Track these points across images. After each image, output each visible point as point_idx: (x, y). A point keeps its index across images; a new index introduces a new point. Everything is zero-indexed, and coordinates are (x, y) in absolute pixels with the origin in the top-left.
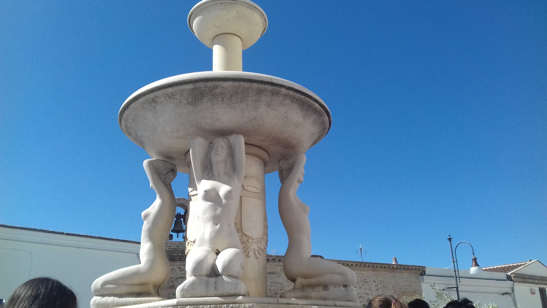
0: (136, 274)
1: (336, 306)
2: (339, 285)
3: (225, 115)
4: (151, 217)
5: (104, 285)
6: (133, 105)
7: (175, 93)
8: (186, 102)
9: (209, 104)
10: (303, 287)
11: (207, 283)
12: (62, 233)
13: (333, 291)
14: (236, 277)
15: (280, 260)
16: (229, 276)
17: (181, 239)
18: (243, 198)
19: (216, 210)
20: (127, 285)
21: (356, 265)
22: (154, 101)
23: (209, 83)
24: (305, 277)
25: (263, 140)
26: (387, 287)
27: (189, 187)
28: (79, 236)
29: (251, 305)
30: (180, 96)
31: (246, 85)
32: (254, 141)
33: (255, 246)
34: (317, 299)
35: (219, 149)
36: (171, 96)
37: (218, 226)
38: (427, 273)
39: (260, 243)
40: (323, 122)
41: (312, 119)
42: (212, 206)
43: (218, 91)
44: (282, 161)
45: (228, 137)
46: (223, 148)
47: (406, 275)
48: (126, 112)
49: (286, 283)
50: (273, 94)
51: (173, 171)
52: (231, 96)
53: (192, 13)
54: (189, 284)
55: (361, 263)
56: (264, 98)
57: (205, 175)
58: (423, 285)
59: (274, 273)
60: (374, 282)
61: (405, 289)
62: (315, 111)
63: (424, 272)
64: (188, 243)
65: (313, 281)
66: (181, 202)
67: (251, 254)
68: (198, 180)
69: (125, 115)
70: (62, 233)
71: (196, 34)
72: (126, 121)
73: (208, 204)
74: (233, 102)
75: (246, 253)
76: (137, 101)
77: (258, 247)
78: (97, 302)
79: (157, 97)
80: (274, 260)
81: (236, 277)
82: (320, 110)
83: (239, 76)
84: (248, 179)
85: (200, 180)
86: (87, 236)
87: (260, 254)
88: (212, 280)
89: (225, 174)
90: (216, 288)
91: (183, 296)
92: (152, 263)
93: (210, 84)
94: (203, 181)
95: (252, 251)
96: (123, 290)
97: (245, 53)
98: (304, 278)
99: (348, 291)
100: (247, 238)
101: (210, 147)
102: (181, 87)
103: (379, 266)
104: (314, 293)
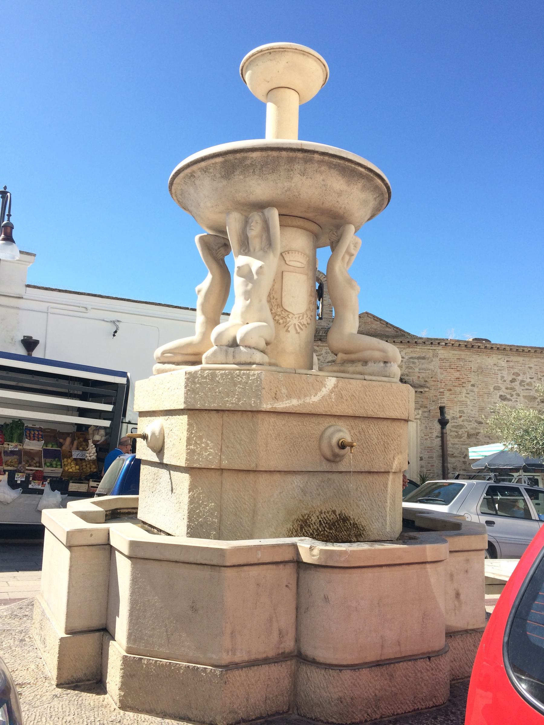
0: (189, 345)
1: (365, 380)
3: (259, 188)
4: (203, 293)
6: (177, 180)
7: (209, 167)
8: (220, 176)
9: (241, 177)
10: (344, 362)
11: (227, 352)
12: (187, 309)
13: (371, 367)
14: (250, 347)
15: (432, 343)
18: (283, 254)
19: (247, 285)
21: (535, 351)
22: (192, 175)
23: (238, 154)
24: (346, 352)
25: (305, 211)
29: (259, 372)
31: (275, 154)
33: (296, 322)
34: (353, 373)
36: (205, 170)
37: (249, 300)
39: (303, 318)
41: (360, 185)
42: (244, 281)
43: (248, 162)
49: (439, 370)
50: (306, 161)
52: (262, 166)
53: (243, 67)
56: (296, 166)
57: (242, 251)
59: (424, 358)
65: (353, 356)
70: (187, 309)
71: (250, 89)
73: (242, 279)
74: (265, 173)
75: (286, 328)
77: (300, 322)
79: (194, 172)
80: (424, 343)
81: (250, 347)
82: (367, 174)
83: (267, 145)
84: (290, 254)
85: (237, 256)
88: (231, 350)
89: (261, 249)
90: (234, 357)
91: (207, 363)
93: (238, 156)
95: (292, 325)
96: (179, 358)
97: (301, 107)
99: (386, 367)
100: (287, 313)
101: (246, 222)
104: (351, 368)
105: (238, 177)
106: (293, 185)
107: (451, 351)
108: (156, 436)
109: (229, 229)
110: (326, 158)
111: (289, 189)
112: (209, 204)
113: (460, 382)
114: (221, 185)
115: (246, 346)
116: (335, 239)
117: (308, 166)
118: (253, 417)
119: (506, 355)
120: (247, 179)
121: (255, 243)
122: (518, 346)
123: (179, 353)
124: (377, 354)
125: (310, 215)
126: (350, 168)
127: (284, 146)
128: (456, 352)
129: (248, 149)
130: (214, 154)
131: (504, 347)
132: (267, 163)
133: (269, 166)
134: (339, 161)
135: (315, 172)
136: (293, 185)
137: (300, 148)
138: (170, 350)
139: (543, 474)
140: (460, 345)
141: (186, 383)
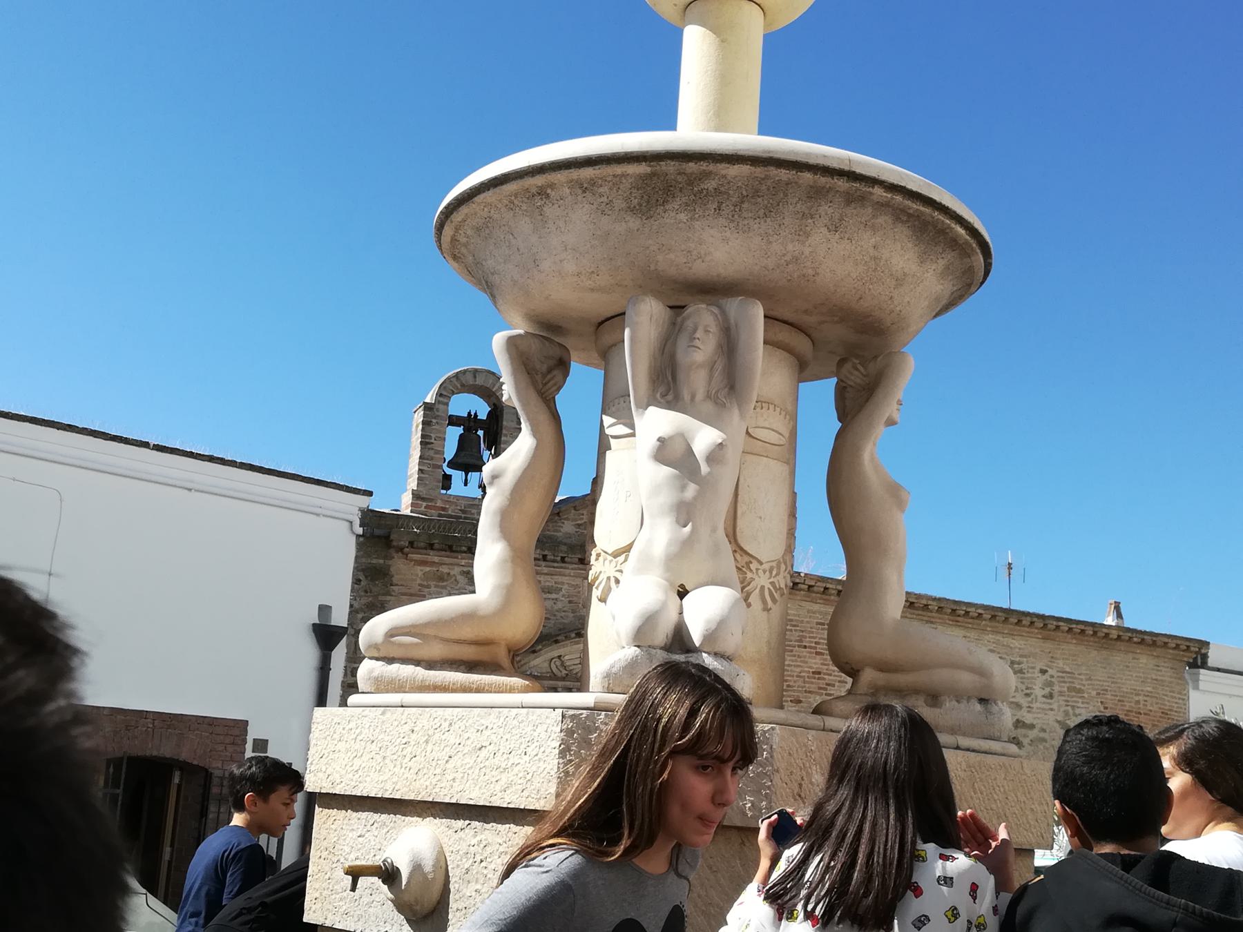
0: (469, 617)
1: (958, 748)
2: (969, 699)
3: (721, 248)
4: (508, 480)
5: (392, 636)
9: (683, 216)
12: (145, 445)
16: (716, 655)
17: (473, 491)
19: (683, 488)
20: (447, 641)
21: (994, 617)
22: (542, 192)
24: (884, 667)
25: (806, 312)
26: (1080, 691)
27: (604, 412)
28: (191, 455)
30: (611, 189)
31: (784, 174)
32: (787, 314)
35: (697, 335)
36: (586, 188)
37: (688, 528)
38: (1211, 662)
40: (970, 270)
41: (942, 263)
42: (676, 477)
44: (848, 366)
45: (723, 302)
46: (707, 331)
47: (1144, 661)
48: (464, 210)
50: (851, 199)
51: (563, 365)
54: (623, 664)
55: (1009, 612)
57: (658, 395)
58: (1193, 694)
60: (1043, 672)
61: (1138, 702)
62: (954, 243)
63: (1205, 657)
64: (598, 555)
66: (480, 381)
67: (754, 599)
68: (638, 407)
69: (457, 217)
70: (145, 445)
72: (457, 229)
73: (666, 471)
76: (497, 190)
78: (375, 674)
79: (552, 186)
82: (967, 242)
86: (211, 459)
87: (774, 600)
92: (508, 595)
93: (692, 167)
94: (651, 409)
96: (436, 651)
98: (881, 670)
99: (990, 713)
100: (747, 559)
102: (618, 169)
103: (1064, 627)
105: (674, 216)
106: (807, 251)
107: (803, 604)
108: (425, 875)
109: (632, 340)
110: (898, 198)
111: (796, 259)
112: (570, 267)
113: (822, 683)
114: (620, 228)
115: (716, 654)
116: (858, 381)
117: (850, 211)
118: (743, 843)
119: (927, 622)
120: (697, 224)
121: (697, 381)
122: (955, 602)
123: (436, 637)
124: (966, 679)
125: (810, 320)
126: (939, 226)
127: (812, 161)
128: (816, 607)
129: (721, 155)
130: (626, 154)
131: (924, 602)
132: (756, 193)
133: (759, 200)
134: (922, 208)
135: (862, 226)
136: (807, 251)
137: (847, 168)
138: (413, 626)
139: (993, 924)
140: (826, 588)
141: (563, 742)
